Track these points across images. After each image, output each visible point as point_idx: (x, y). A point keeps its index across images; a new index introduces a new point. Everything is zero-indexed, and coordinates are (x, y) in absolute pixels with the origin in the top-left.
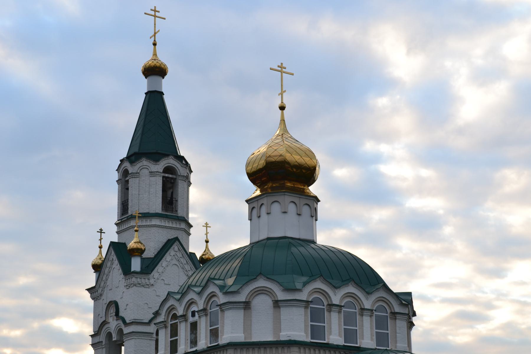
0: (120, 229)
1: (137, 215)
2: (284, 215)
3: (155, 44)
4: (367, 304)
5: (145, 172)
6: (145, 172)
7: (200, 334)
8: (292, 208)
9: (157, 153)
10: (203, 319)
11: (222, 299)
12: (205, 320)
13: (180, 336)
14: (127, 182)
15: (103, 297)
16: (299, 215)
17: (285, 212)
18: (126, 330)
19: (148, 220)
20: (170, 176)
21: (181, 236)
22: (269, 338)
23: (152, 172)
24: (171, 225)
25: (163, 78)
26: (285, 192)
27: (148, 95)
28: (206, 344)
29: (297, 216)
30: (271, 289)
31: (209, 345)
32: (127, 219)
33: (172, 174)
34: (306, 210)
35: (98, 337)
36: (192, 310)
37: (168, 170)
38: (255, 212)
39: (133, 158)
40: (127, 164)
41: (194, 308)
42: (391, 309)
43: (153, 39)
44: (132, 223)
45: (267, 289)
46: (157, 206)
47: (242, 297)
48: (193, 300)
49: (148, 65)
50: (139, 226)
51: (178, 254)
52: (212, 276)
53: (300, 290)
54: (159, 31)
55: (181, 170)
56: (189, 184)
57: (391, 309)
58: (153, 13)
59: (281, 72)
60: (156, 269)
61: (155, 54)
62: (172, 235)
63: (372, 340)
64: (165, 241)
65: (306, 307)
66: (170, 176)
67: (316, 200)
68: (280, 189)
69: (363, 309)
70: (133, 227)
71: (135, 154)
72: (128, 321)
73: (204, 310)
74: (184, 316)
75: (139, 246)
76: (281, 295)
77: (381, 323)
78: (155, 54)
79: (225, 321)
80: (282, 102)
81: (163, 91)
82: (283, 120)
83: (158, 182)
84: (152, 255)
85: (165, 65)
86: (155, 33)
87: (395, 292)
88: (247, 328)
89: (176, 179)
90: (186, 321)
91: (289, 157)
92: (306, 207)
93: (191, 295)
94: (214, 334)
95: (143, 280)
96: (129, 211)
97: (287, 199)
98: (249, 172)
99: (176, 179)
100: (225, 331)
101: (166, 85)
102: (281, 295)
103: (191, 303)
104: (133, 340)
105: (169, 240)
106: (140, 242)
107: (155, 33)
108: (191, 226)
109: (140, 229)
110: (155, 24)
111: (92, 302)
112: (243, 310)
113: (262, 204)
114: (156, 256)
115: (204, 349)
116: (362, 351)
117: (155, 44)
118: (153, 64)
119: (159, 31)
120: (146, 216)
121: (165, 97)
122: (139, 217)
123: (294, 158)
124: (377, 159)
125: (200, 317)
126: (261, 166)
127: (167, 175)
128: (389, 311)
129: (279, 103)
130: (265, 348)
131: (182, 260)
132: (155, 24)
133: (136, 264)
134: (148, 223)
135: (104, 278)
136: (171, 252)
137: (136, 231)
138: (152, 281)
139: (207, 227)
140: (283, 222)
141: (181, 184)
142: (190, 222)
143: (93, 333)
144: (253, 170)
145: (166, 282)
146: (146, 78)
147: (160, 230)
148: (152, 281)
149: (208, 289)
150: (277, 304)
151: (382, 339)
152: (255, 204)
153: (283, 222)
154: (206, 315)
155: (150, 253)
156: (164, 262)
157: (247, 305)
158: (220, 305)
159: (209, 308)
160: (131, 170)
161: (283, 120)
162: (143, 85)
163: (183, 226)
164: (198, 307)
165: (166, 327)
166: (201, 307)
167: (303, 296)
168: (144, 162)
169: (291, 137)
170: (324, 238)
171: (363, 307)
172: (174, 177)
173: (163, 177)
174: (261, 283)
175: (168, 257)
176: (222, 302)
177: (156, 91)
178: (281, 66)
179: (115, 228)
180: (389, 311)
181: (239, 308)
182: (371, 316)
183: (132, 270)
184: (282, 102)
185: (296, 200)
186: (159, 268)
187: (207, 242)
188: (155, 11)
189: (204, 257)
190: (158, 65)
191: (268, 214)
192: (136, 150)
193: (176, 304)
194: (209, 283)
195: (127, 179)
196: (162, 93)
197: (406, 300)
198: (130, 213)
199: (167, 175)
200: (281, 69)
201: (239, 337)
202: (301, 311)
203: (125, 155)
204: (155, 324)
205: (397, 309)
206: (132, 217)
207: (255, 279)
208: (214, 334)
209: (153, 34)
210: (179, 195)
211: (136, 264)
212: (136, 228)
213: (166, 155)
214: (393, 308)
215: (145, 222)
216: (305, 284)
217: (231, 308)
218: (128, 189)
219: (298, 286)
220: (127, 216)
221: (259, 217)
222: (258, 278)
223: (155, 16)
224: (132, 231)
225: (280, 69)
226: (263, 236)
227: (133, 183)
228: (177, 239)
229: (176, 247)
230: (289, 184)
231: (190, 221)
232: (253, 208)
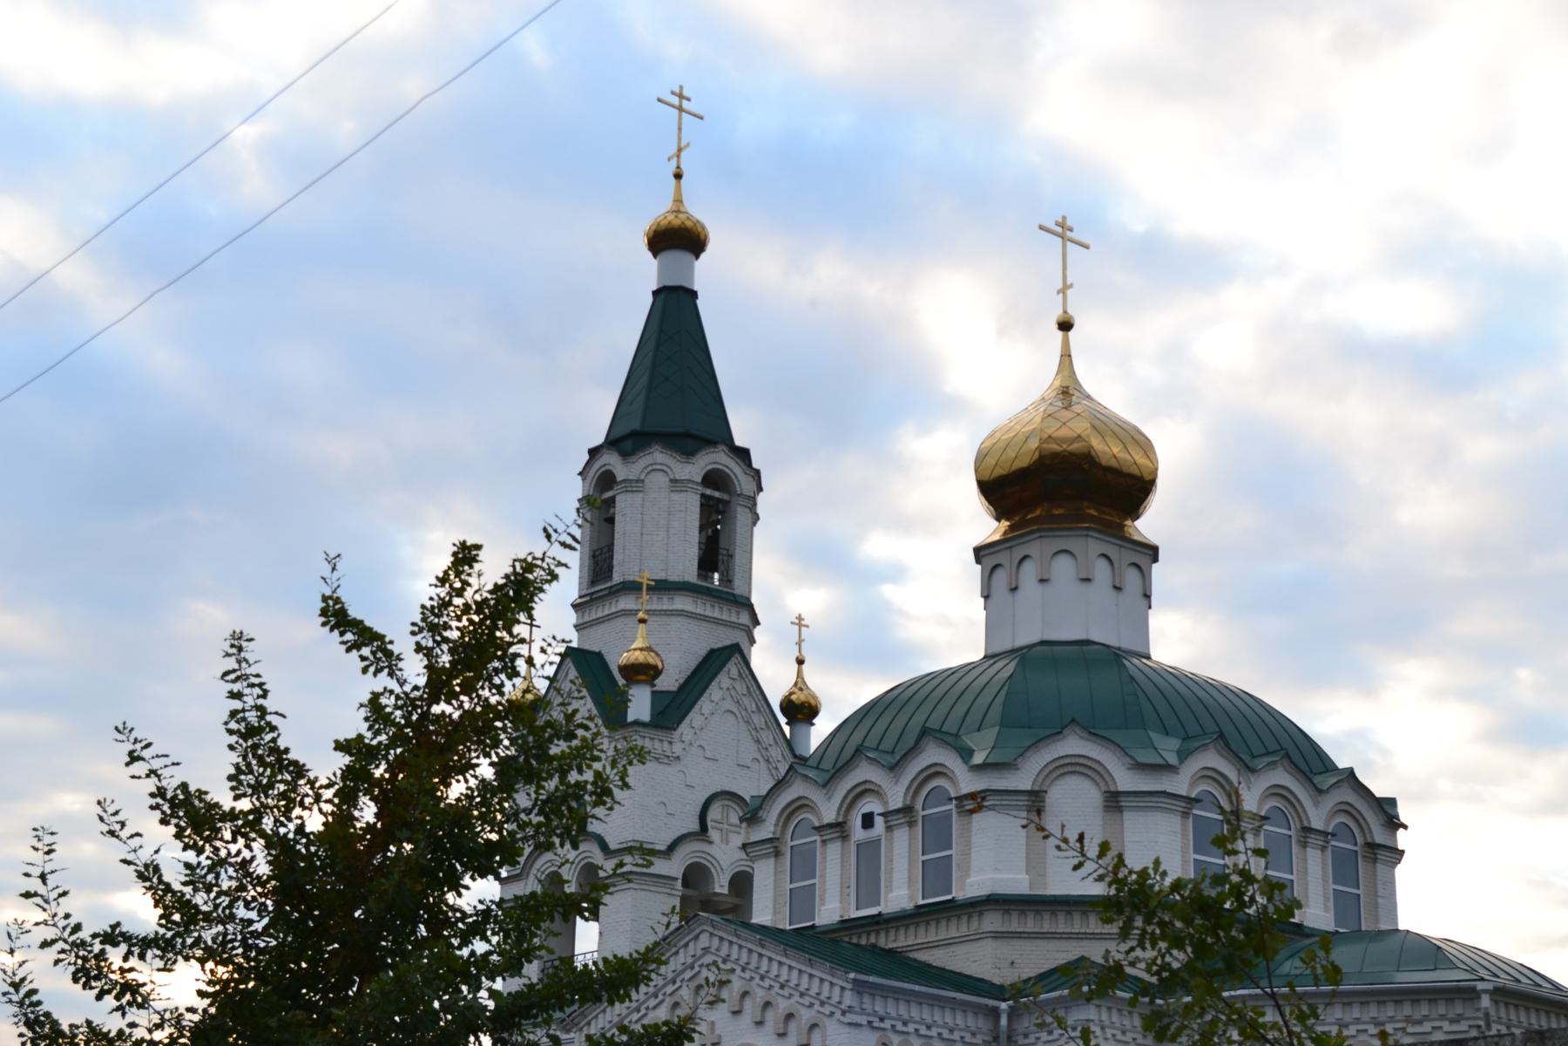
0: (587, 619)
1: (645, 582)
2: (1083, 587)
3: (678, 176)
4: (1317, 820)
5: (660, 480)
6: (660, 480)
7: (890, 872)
8: (1101, 570)
9: (687, 435)
10: (902, 837)
11: (968, 783)
12: (906, 837)
13: (823, 876)
14: (612, 501)
17: (1088, 580)
19: (665, 599)
20: (717, 494)
21: (744, 646)
24: (716, 615)
25: (697, 257)
26: (1088, 529)
27: (662, 296)
28: (911, 898)
29: (1114, 592)
31: (921, 902)
32: (592, 600)
33: (717, 489)
34: (1132, 576)
35: (522, 884)
36: (866, 810)
37: (714, 479)
38: (1001, 577)
39: (628, 445)
40: (611, 460)
41: (871, 805)
43: (674, 162)
44: (626, 602)
45: (1089, 763)
46: (686, 567)
47: (1023, 780)
48: (868, 786)
49: (665, 223)
50: (648, 612)
51: (738, 687)
52: (934, 723)
53: (1167, 768)
54: (688, 145)
55: (744, 484)
56: (756, 518)
58: (675, 100)
59: (1062, 237)
60: (687, 720)
61: (678, 200)
62: (723, 638)
63: (1326, 909)
64: (703, 652)
65: (1185, 815)
66: (717, 494)
67: (1153, 552)
68: (1073, 521)
69: (1307, 830)
70: (634, 612)
71: (633, 435)
72: (613, 846)
73: (907, 810)
74: (839, 828)
75: (652, 659)
77: (1344, 869)
78: (678, 200)
79: (975, 839)
80: (1065, 312)
81: (697, 286)
83: (690, 505)
84: (673, 687)
86: (680, 150)
88: (1035, 864)
89: (727, 503)
90: (845, 837)
91: (1097, 444)
92: (1133, 572)
93: (865, 772)
94: (937, 872)
95: (657, 744)
97: (1091, 546)
98: (986, 477)
99: (727, 503)
101: (705, 274)
102: (1126, 780)
103: (864, 790)
104: (631, 892)
105: (712, 652)
106: (649, 649)
107: (680, 150)
109: (651, 619)
110: (680, 129)
112: (772, 860)
113: (1025, 557)
114: (682, 687)
115: (904, 911)
116: (1308, 936)
117: (678, 176)
118: (677, 222)
119: (688, 145)
120: (662, 587)
121: (701, 303)
122: (650, 588)
123: (1108, 450)
124: (895, 573)
125: (889, 829)
126: (1024, 462)
127: (708, 492)
128: (1360, 840)
129: (1056, 314)
130: (1084, 913)
131: (746, 701)
132: (680, 129)
133: (640, 705)
136: (723, 680)
137: (642, 621)
138: (677, 748)
139: (800, 625)
140: (1067, 603)
141: (742, 515)
144: (999, 472)
145: (709, 754)
146: (655, 256)
147: (694, 626)
148: (677, 748)
149: (921, 757)
150: (1114, 801)
151: (1346, 905)
153: (1067, 603)
154: (911, 824)
155: (669, 681)
156: (704, 705)
157: (1035, 801)
158: (959, 799)
159: (919, 805)
160: (621, 471)
161: (1066, 356)
162: (647, 273)
163: (744, 619)
164: (886, 803)
165: (777, 854)
166: (896, 802)
167: (1180, 784)
168: (657, 455)
169: (1088, 397)
172: (726, 497)
173: (703, 496)
174: (1073, 745)
175: (715, 692)
176: (964, 792)
178: (1062, 225)
179: (572, 617)
180: (1360, 840)
182: (1323, 849)
183: (630, 719)
184: (1065, 312)
185: (1112, 552)
186: (694, 718)
187: (800, 662)
188: (681, 96)
189: (794, 697)
190: (689, 224)
192: (635, 424)
193: (815, 795)
194: (925, 740)
195: (609, 494)
196: (694, 294)
198: (617, 578)
199: (708, 492)
200: (1062, 231)
201: (1017, 882)
202: (1174, 822)
203: (599, 439)
206: (631, 587)
207: (1058, 733)
208: (937, 872)
209: (675, 150)
210: (738, 542)
211: (640, 705)
212: (641, 615)
213: (710, 443)
215: (665, 603)
216: (1184, 755)
218: (611, 521)
219: (1172, 759)
221: (1014, 589)
222: (1066, 732)
223: (680, 109)
224: (632, 621)
225: (1059, 230)
226: (1026, 637)
227: (626, 506)
229: (732, 667)
230: (1093, 512)
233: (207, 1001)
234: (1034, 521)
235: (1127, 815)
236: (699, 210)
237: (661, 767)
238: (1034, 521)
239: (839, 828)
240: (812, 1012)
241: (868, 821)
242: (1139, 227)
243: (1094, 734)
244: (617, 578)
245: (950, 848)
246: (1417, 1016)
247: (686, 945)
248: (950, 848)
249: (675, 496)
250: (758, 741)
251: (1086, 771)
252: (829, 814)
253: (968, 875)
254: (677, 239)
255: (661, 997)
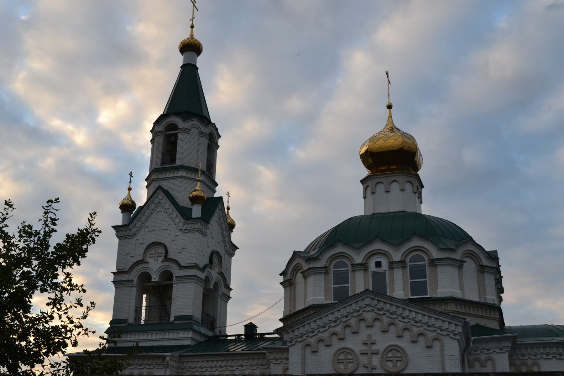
15: (136, 237)
16: (403, 190)
18: (176, 272)
22: (476, 299)
23: (203, 133)
30: (422, 247)
35: (128, 275)
38: (369, 190)
42: (479, 262)
57: (479, 262)
76: (436, 254)
79: (439, 276)
82: (390, 117)
85: (199, 43)
87: (486, 250)
96: (177, 162)
97: (400, 178)
100: (439, 285)
101: (201, 62)
108: (217, 185)
111: (117, 240)
118: (192, 41)
121: (199, 71)
129: (386, 103)
131: (221, 218)
134: (159, 176)
135: (143, 219)
142: (216, 180)
143: (116, 271)
152: (369, 183)
153: (394, 200)
157: (460, 264)
160: (181, 124)
161: (390, 117)
162: (179, 60)
165: (326, 273)
170: (426, 209)
171: (431, 258)
174: (378, 246)
177: (190, 64)
181: (454, 266)
191: (373, 193)
197: (493, 256)
198: (178, 163)
204: (301, 273)
205: (485, 262)
208: (418, 287)
214: (481, 261)
216: (458, 246)
217: (449, 265)
220: (173, 165)
228: (160, 187)
231: (216, 180)
232: (368, 186)
233: (51, 306)
234: (393, 170)
235: (485, 274)
236: (198, 37)
237: (202, 237)
238: (393, 170)
239: (364, 266)
240: (435, 334)
241: (378, 264)
242: (32, 124)
243: (384, 241)
244: (178, 163)
245: (426, 278)
246: (253, 364)
247: (357, 302)
248: (426, 278)
249: (200, 138)
250: (223, 234)
251: (472, 256)
252: (358, 259)
253: (438, 289)
254: (191, 48)
255: (338, 322)
